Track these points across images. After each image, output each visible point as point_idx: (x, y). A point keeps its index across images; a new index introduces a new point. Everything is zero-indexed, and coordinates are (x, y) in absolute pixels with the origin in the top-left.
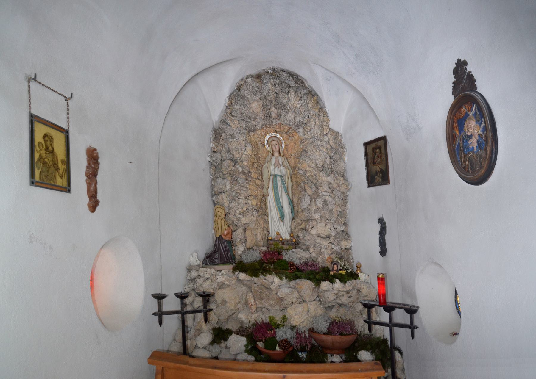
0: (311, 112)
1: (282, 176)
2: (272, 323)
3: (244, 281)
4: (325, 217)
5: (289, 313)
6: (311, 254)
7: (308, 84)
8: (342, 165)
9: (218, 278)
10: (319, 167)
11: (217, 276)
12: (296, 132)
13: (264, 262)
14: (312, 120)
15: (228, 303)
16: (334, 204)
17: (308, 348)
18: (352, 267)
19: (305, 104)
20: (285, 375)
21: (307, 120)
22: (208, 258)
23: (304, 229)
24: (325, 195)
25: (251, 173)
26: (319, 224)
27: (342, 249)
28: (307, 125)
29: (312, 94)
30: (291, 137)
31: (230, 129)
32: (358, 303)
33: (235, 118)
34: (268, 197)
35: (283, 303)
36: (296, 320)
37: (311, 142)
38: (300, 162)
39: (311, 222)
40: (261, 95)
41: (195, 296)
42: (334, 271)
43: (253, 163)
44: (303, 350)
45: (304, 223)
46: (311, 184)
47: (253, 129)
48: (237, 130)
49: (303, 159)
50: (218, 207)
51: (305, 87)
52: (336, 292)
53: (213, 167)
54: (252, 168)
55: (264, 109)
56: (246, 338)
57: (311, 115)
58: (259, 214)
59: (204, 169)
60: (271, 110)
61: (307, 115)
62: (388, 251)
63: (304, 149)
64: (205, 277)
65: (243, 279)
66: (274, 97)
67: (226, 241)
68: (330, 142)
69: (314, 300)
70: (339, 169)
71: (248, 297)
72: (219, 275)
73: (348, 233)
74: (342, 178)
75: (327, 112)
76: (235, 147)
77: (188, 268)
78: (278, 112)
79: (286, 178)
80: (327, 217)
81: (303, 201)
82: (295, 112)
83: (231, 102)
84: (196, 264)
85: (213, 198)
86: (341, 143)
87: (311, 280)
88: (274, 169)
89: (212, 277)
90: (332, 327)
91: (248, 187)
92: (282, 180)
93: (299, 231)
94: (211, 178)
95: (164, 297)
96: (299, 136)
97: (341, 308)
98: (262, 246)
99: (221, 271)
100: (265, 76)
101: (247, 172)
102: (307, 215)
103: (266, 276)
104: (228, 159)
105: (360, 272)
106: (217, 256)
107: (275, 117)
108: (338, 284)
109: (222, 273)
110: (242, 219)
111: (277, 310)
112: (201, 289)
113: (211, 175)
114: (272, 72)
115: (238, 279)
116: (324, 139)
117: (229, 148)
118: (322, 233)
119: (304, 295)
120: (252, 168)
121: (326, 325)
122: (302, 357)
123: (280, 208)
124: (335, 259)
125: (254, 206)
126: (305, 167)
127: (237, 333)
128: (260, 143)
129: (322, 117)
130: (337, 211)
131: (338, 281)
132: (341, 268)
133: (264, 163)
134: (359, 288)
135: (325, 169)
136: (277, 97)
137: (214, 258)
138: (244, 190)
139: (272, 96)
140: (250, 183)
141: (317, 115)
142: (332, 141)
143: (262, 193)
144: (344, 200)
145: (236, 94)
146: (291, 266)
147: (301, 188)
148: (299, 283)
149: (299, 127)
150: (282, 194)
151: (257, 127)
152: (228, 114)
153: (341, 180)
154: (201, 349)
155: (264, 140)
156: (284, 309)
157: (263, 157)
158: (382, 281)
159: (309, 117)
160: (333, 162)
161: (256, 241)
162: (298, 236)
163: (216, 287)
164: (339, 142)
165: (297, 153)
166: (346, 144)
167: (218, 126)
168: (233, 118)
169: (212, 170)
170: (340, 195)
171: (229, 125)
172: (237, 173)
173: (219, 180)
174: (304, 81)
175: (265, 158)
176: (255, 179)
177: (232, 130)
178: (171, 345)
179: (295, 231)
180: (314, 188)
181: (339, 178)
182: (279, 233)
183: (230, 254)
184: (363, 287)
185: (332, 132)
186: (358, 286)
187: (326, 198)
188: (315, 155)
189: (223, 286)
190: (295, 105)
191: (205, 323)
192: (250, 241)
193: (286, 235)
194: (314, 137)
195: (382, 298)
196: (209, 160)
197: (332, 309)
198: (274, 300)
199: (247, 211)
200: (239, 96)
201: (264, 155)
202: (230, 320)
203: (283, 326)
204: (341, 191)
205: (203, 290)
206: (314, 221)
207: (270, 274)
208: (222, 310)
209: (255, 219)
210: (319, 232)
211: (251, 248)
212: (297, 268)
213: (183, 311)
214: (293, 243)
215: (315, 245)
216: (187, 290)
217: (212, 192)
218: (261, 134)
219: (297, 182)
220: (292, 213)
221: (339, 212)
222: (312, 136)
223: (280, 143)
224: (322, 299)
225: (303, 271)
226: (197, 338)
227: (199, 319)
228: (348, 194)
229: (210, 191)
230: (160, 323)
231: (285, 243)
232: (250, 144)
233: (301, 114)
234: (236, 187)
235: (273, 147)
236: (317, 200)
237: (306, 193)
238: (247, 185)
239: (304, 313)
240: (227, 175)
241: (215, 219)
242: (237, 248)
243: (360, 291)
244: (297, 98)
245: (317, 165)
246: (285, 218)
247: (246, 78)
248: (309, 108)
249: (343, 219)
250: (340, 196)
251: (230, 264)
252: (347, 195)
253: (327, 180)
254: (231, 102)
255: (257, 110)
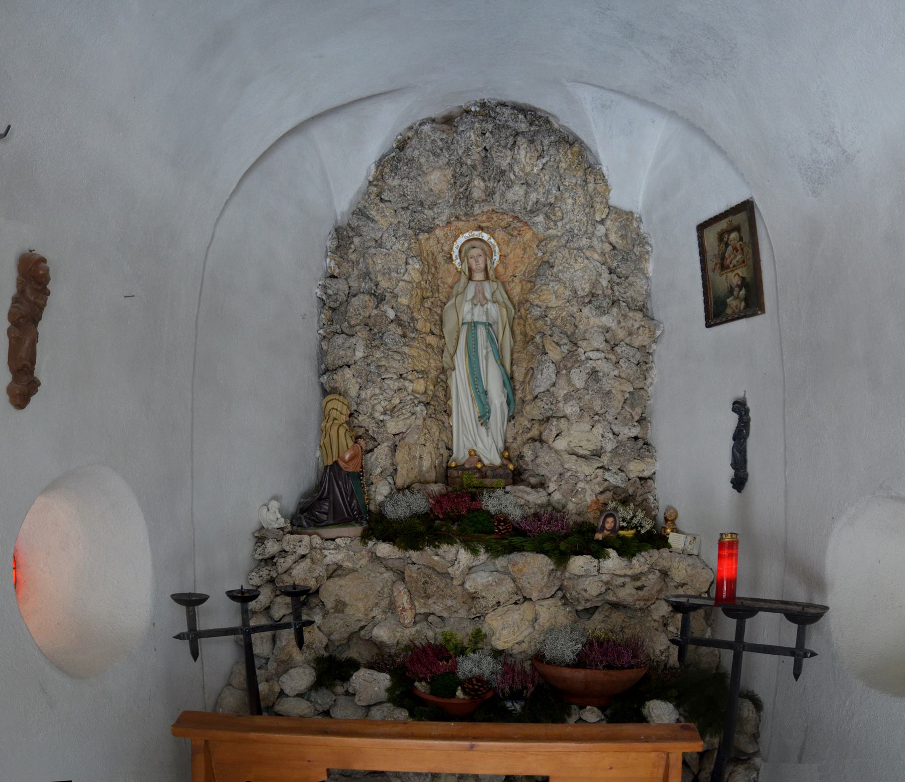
0: (565, 179)
1: (489, 323)
2: (450, 646)
3: (388, 559)
4: (591, 409)
5: (489, 625)
6: (550, 494)
7: (560, 123)
8: (639, 284)
9: (326, 556)
10: (582, 297)
11: (323, 551)
12: (527, 225)
13: (437, 518)
14: (567, 195)
15: (349, 607)
16: (615, 376)
17: (527, 694)
18: (654, 518)
19: (551, 163)
20: (473, 743)
21: (556, 197)
22: (304, 512)
23: (536, 441)
24: (594, 358)
25: (417, 320)
26: (574, 426)
27: (629, 480)
28: (554, 208)
29: (568, 142)
30: (516, 237)
31: (373, 229)
32: (659, 601)
33: (388, 204)
34: (453, 373)
35: (477, 604)
36: (505, 638)
37: (564, 242)
38: (534, 290)
39: (555, 423)
40: (450, 155)
41: (274, 594)
42: (606, 532)
43: (424, 298)
44: (515, 696)
45: (536, 426)
46: (560, 337)
47: (426, 227)
48: (391, 231)
49: (543, 282)
50: (333, 399)
51: (551, 131)
52: (605, 578)
53: (326, 310)
54: (419, 310)
55: (455, 183)
56: (390, 675)
57: (565, 185)
58: (430, 411)
59: (305, 315)
60: (471, 185)
61: (557, 185)
62: (750, 478)
63: (546, 259)
64: (297, 554)
65: (386, 555)
66: (479, 158)
67: (349, 474)
68: (610, 236)
69: (551, 597)
70: (631, 294)
71: (395, 594)
72: (330, 549)
73: (650, 441)
74: (639, 315)
75: (604, 172)
76: (383, 266)
77: (256, 535)
78: (486, 186)
79: (498, 328)
80: (597, 409)
81: (539, 376)
82: (527, 184)
83: (382, 171)
84: (276, 526)
85: (322, 380)
86: (638, 234)
87: (546, 553)
88: (472, 308)
89: (314, 553)
90: (589, 652)
91: (406, 351)
92: (488, 333)
93: (524, 444)
94: (320, 334)
95: (202, 599)
96: (534, 233)
97: (615, 613)
98: (432, 482)
99: (333, 540)
100: (461, 118)
101: (405, 319)
102: (546, 407)
103: (439, 547)
104: (363, 293)
105: (676, 530)
106: (326, 507)
107: (480, 198)
108: (613, 562)
109: (337, 544)
110: (388, 425)
111: (462, 618)
112: (288, 581)
113: (321, 329)
114: (478, 109)
115: (374, 555)
116: (596, 232)
117: (367, 268)
118: (581, 447)
119: (528, 586)
120: (419, 310)
121: (575, 647)
122: (513, 710)
123: (481, 395)
124: (610, 502)
125: (419, 393)
126: (547, 299)
127: (371, 666)
128: (441, 255)
129: (591, 186)
130: (622, 391)
131: (613, 553)
132: (625, 524)
133: (448, 299)
134: (665, 567)
135: (597, 300)
136: (486, 157)
137: (318, 512)
138: (396, 360)
139: (476, 155)
140: (411, 343)
141: (579, 183)
142: (616, 233)
143: (439, 364)
144: (644, 364)
145: (394, 157)
146: (499, 524)
147: (533, 348)
148: (517, 562)
149: (535, 214)
150: (487, 363)
151: (437, 222)
152: (372, 197)
153: (637, 318)
154: (292, 699)
155: (452, 249)
156: (481, 617)
157: (446, 286)
158: (729, 549)
159: (559, 190)
160: (618, 280)
161: (421, 471)
162: (521, 457)
163: (321, 574)
164: (634, 233)
165: (528, 269)
166: (651, 234)
167: (346, 222)
168: (382, 205)
169: (323, 316)
170: (631, 354)
171: (373, 221)
172: (384, 321)
173: (339, 340)
174: (551, 119)
175: (452, 288)
176: (425, 333)
177: (379, 230)
178: (222, 695)
179: (515, 445)
180: (566, 344)
181: (631, 314)
182: (475, 451)
183: (357, 502)
184: (676, 565)
185: (616, 213)
186: (664, 563)
187: (595, 365)
188: (572, 270)
189: (339, 572)
190: (528, 169)
191: (298, 649)
192: (405, 473)
193: (492, 454)
194: (571, 231)
195: (725, 589)
196: (318, 294)
197: (592, 614)
198: (455, 599)
199: (401, 405)
200: (400, 161)
201: (450, 281)
202: (355, 640)
203: (474, 652)
204: (636, 344)
205: (292, 582)
206: (562, 419)
207: (448, 544)
208: (337, 621)
209: (419, 423)
210: (572, 445)
211: (406, 488)
212: (515, 529)
213: (249, 625)
214: (508, 473)
215: (561, 474)
216: (256, 581)
217: (319, 365)
218: (446, 235)
219: (525, 335)
220: (508, 404)
221: (627, 395)
222: (566, 230)
223: (488, 253)
224: (571, 594)
225: (528, 534)
226: (281, 678)
227: (283, 641)
228: (654, 350)
229: (316, 363)
230: (195, 654)
231: (489, 473)
232: (419, 258)
233: (542, 187)
234: (378, 352)
235: (472, 261)
236: (573, 371)
237: (545, 357)
238: (404, 348)
239: (525, 624)
240: (358, 328)
241: (323, 425)
242: (373, 489)
243: (669, 573)
244: (533, 155)
245: (576, 293)
246: (491, 419)
247: (420, 125)
248: (562, 171)
249: (637, 409)
250: (633, 356)
251: (356, 525)
252: (650, 351)
253: (601, 324)
254: (382, 171)
255: (439, 187)
